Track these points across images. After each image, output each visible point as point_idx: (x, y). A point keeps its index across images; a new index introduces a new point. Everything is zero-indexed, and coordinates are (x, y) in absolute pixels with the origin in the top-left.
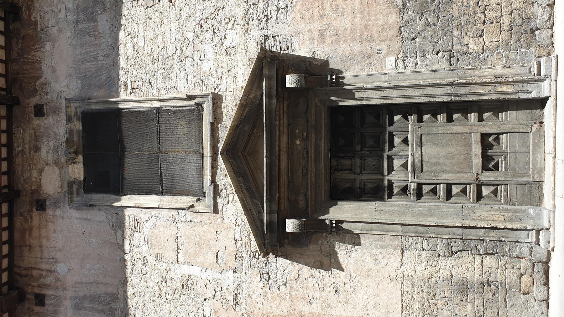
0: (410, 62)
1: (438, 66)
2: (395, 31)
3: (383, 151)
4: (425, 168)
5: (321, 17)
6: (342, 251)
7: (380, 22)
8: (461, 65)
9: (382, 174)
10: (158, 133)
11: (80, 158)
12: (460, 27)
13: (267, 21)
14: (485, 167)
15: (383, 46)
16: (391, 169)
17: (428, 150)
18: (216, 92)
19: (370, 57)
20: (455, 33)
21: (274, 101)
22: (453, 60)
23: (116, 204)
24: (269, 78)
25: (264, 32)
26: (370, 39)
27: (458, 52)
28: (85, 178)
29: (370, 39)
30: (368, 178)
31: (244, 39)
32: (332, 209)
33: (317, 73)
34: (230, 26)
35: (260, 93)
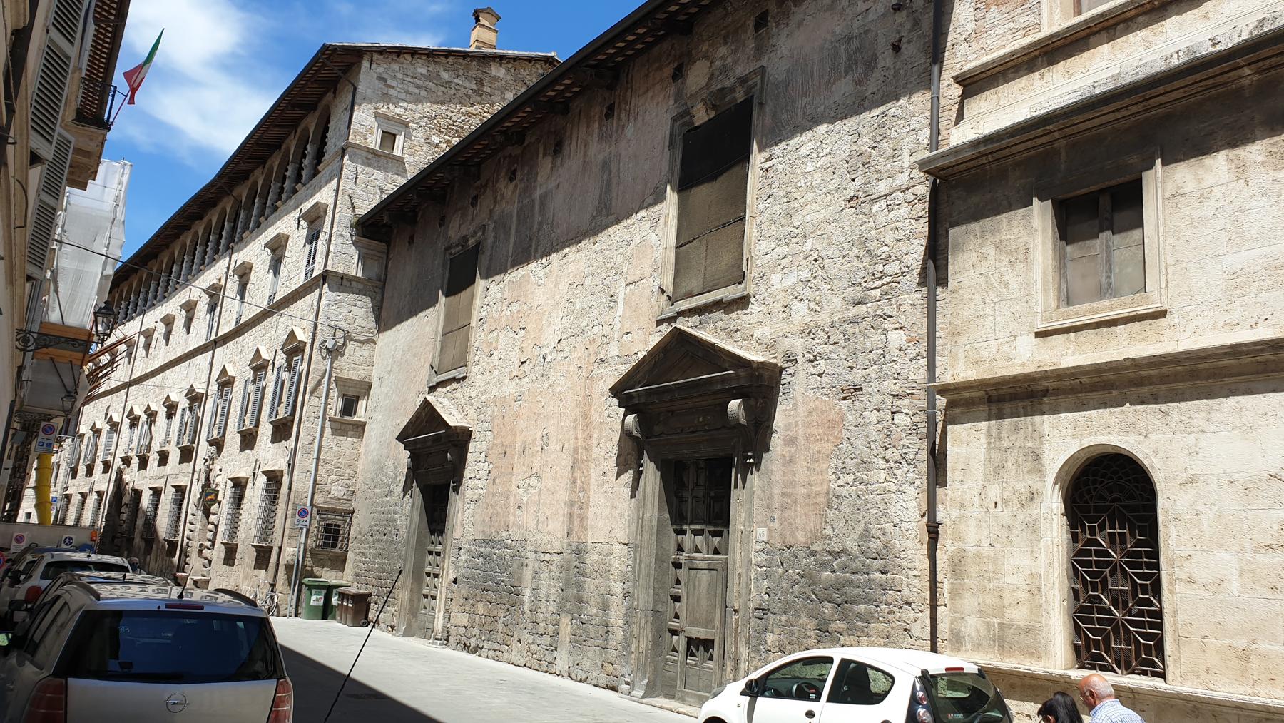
0: (761, 558)
1: (754, 593)
2: (790, 540)
3: (709, 523)
4: (693, 572)
5: (807, 438)
6: (628, 477)
7: (798, 521)
8: (753, 622)
9: (692, 523)
10: (724, 225)
11: (713, 114)
12: (789, 624)
13: (811, 361)
14: (690, 641)
15: (777, 525)
16: (697, 533)
17: (705, 576)
18: (752, 300)
19: (768, 506)
20: (784, 618)
21: (719, 387)
22: (760, 613)
23: (669, 187)
24: (738, 377)
25: (800, 358)
26: (784, 508)
27: (768, 620)
28: (698, 127)
29: (784, 508)
30: (688, 507)
31: (794, 330)
32: (653, 464)
33: (754, 439)
34: (812, 305)
35: (727, 366)
